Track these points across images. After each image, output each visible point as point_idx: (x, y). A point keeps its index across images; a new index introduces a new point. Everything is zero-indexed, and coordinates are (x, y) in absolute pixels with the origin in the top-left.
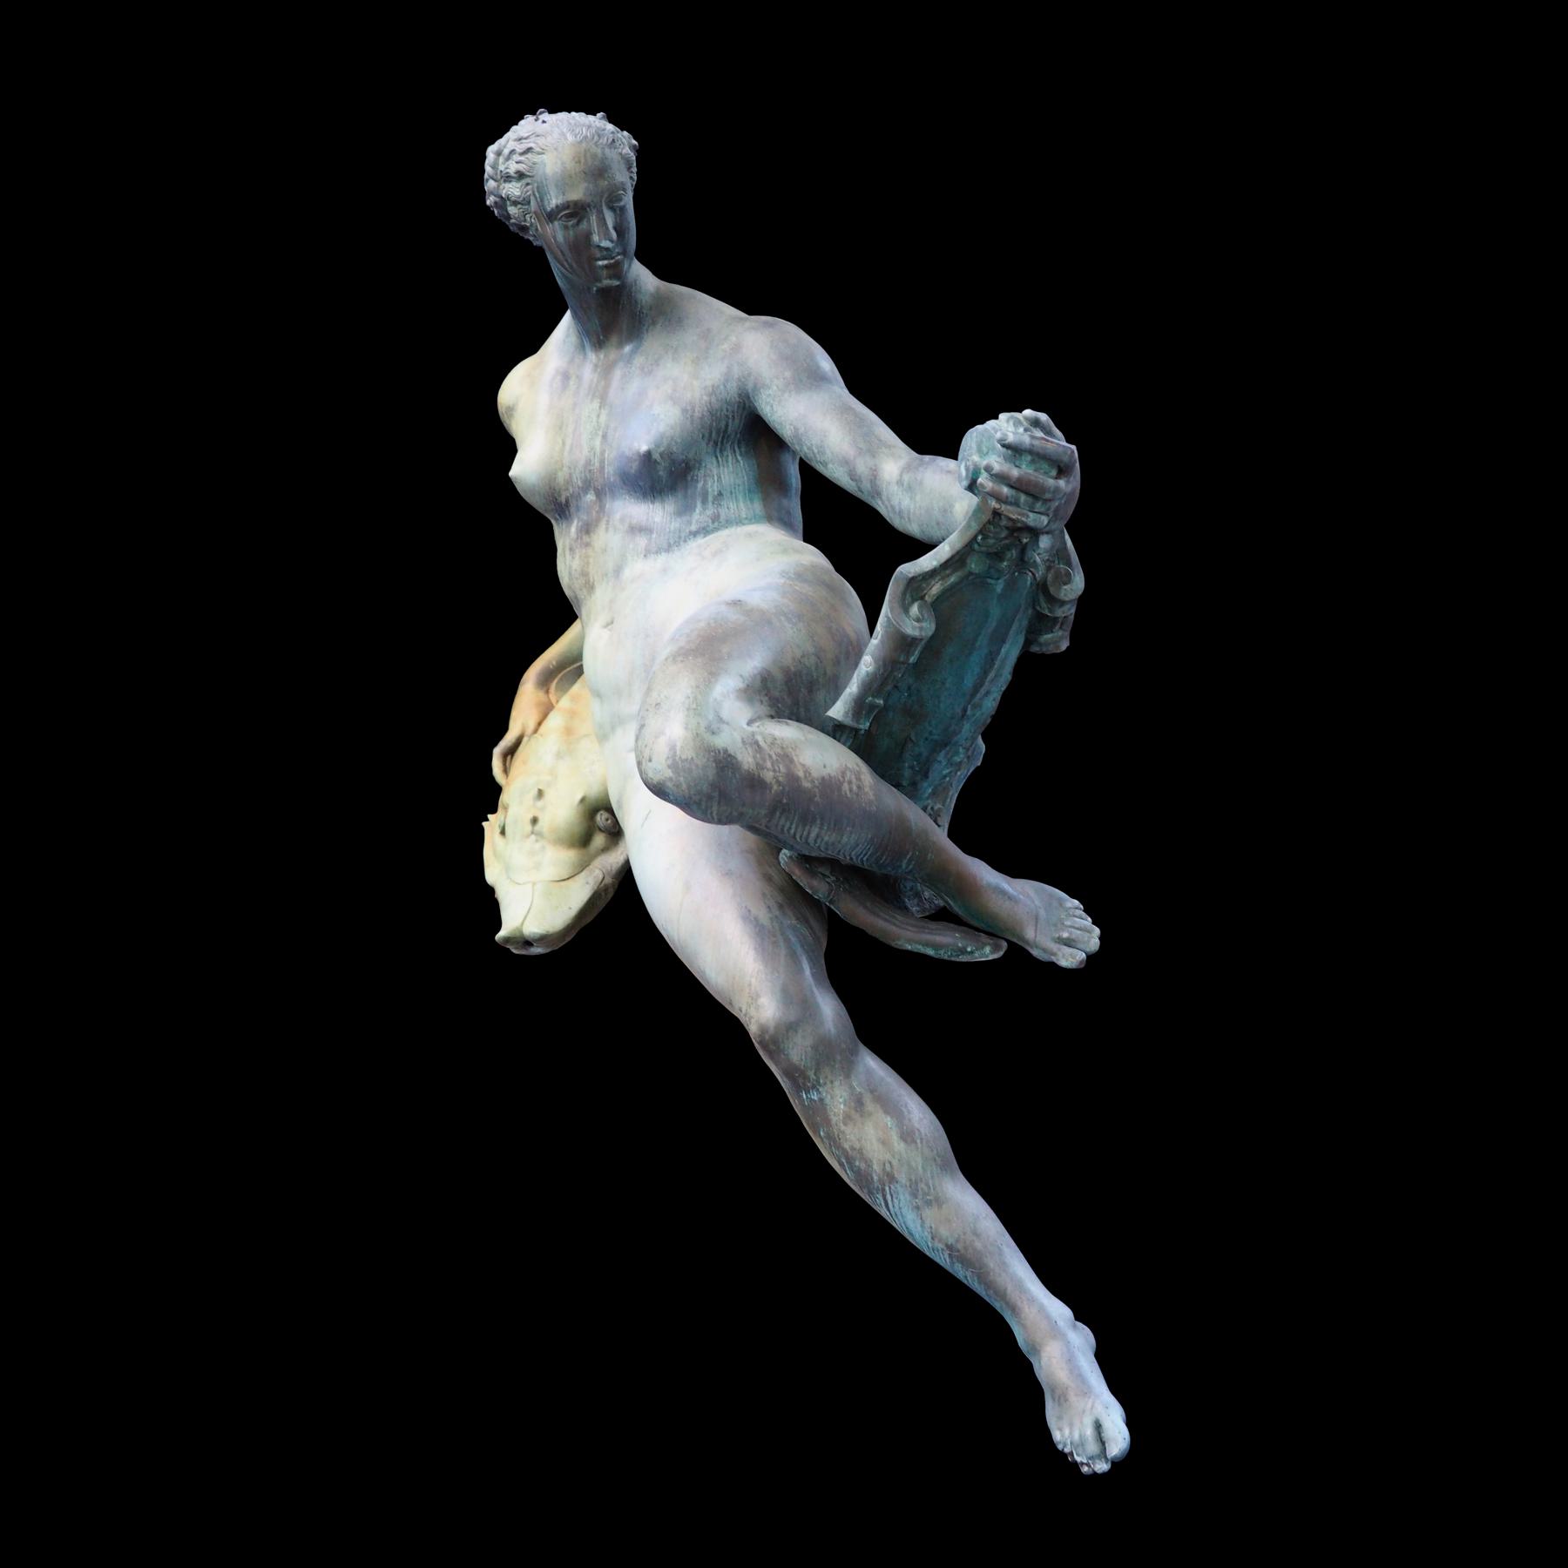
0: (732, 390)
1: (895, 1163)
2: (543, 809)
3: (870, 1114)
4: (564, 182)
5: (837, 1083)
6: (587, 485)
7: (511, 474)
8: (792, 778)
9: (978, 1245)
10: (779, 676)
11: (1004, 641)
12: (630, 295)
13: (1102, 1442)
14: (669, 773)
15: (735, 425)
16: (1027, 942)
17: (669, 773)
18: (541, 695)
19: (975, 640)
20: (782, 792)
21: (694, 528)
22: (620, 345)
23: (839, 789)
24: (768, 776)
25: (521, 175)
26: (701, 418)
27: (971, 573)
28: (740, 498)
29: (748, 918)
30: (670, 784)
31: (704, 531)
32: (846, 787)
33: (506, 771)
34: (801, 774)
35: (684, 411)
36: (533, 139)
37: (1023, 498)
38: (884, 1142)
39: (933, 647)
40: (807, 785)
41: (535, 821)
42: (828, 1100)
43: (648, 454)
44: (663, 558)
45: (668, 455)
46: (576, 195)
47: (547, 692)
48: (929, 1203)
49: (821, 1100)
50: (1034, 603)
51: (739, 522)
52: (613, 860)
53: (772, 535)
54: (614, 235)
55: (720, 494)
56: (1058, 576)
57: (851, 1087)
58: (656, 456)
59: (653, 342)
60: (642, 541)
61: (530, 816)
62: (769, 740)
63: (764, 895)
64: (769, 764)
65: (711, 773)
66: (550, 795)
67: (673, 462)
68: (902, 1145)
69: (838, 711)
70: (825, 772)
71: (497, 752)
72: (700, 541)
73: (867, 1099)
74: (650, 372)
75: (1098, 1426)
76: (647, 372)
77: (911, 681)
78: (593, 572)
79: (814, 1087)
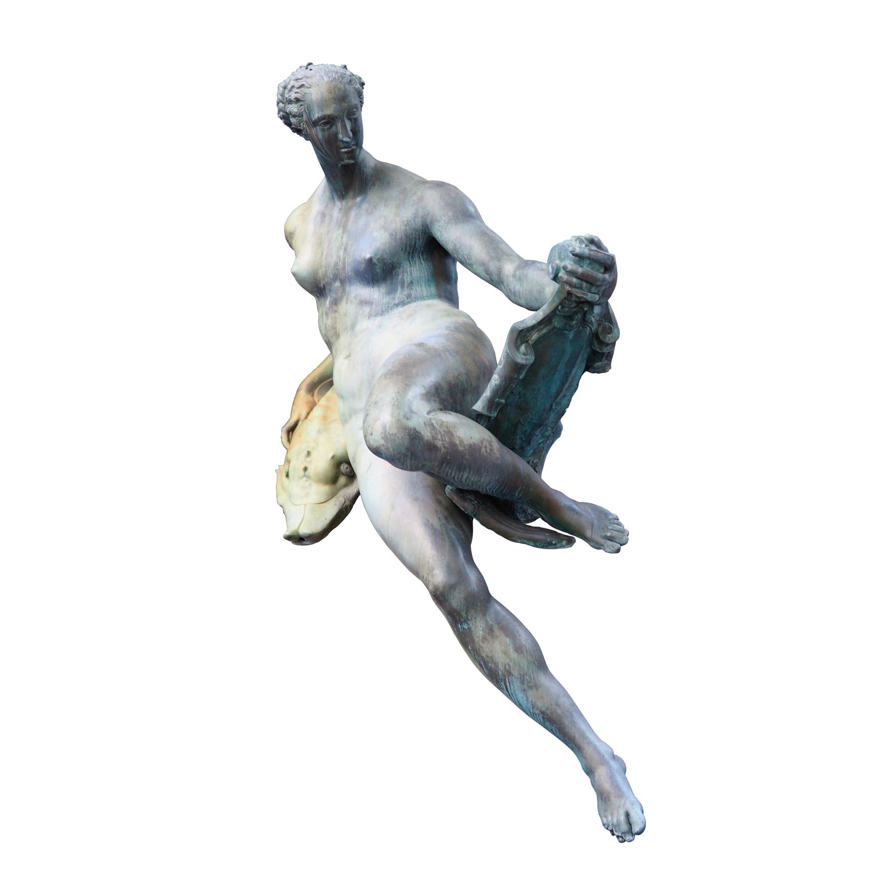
0: (418, 223)
1: (511, 664)
2: (310, 462)
3: (497, 637)
4: (322, 104)
5: (478, 619)
6: (336, 277)
8: (453, 444)
9: (559, 711)
10: (445, 386)
11: (574, 367)
12: (360, 169)
14: (382, 442)
15: (420, 243)
17: (382, 442)
18: (309, 397)
19: (557, 366)
20: (447, 453)
21: (396, 302)
22: (355, 197)
23: (480, 451)
24: (439, 443)
25: (298, 100)
26: (401, 239)
27: (555, 328)
28: (423, 284)
29: (427, 525)
30: (383, 448)
31: (403, 303)
32: (483, 450)
34: (458, 442)
35: (391, 235)
36: (304, 79)
37: (584, 284)
38: (505, 653)
39: (533, 370)
40: (461, 448)
41: (305, 469)
42: (473, 629)
44: (379, 319)
45: (382, 260)
46: (329, 111)
47: (313, 395)
48: (531, 688)
49: (469, 628)
51: (422, 298)
54: (351, 134)
55: (412, 282)
56: (604, 329)
57: (487, 621)
58: (375, 261)
59: (373, 195)
60: (367, 309)
61: (303, 466)
62: (440, 423)
63: (437, 511)
64: (439, 437)
65: (407, 442)
66: (314, 454)
67: (385, 264)
68: (516, 654)
69: (479, 406)
70: (471, 441)
72: (400, 309)
73: (496, 628)
74: (372, 213)
76: (370, 213)
77: (520, 389)
78: (339, 327)
79: (465, 621)
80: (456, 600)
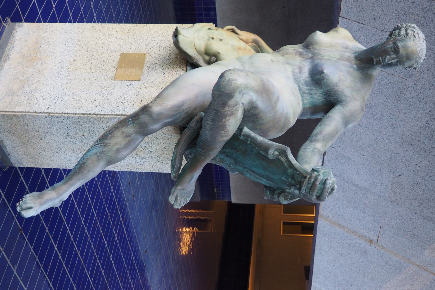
1: (110, 147)
3: (124, 139)
5: (134, 129)
6: (314, 54)
7: (317, 31)
8: (226, 116)
9: (85, 172)
10: (256, 112)
11: (267, 180)
14: (227, 79)
15: (332, 99)
16: (176, 187)
17: (227, 79)
18: (251, 40)
22: (356, 64)
23: (223, 130)
24: (226, 109)
25: (407, 34)
28: (310, 100)
29: (184, 103)
30: (224, 79)
31: (300, 90)
32: (223, 132)
33: (228, 30)
34: (227, 119)
35: (336, 84)
36: (418, 38)
37: (310, 185)
38: (116, 144)
40: (224, 120)
41: (213, 38)
42: (129, 127)
43: (323, 73)
45: (323, 79)
46: (401, 51)
47: (252, 42)
48: (98, 157)
49: (129, 125)
50: (279, 189)
51: (303, 100)
53: (299, 110)
54: (389, 62)
55: (311, 94)
56: (287, 196)
57: (133, 134)
58: (323, 75)
59: (357, 74)
60: (297, 71)
63: (191, 107)
64: (230, 109)
65: (227, 92)
67: (321, 80)
71: (234, 27)
74: (348, 73)
75: (30, 208)
79: (133, 122)
80: (144, 118)
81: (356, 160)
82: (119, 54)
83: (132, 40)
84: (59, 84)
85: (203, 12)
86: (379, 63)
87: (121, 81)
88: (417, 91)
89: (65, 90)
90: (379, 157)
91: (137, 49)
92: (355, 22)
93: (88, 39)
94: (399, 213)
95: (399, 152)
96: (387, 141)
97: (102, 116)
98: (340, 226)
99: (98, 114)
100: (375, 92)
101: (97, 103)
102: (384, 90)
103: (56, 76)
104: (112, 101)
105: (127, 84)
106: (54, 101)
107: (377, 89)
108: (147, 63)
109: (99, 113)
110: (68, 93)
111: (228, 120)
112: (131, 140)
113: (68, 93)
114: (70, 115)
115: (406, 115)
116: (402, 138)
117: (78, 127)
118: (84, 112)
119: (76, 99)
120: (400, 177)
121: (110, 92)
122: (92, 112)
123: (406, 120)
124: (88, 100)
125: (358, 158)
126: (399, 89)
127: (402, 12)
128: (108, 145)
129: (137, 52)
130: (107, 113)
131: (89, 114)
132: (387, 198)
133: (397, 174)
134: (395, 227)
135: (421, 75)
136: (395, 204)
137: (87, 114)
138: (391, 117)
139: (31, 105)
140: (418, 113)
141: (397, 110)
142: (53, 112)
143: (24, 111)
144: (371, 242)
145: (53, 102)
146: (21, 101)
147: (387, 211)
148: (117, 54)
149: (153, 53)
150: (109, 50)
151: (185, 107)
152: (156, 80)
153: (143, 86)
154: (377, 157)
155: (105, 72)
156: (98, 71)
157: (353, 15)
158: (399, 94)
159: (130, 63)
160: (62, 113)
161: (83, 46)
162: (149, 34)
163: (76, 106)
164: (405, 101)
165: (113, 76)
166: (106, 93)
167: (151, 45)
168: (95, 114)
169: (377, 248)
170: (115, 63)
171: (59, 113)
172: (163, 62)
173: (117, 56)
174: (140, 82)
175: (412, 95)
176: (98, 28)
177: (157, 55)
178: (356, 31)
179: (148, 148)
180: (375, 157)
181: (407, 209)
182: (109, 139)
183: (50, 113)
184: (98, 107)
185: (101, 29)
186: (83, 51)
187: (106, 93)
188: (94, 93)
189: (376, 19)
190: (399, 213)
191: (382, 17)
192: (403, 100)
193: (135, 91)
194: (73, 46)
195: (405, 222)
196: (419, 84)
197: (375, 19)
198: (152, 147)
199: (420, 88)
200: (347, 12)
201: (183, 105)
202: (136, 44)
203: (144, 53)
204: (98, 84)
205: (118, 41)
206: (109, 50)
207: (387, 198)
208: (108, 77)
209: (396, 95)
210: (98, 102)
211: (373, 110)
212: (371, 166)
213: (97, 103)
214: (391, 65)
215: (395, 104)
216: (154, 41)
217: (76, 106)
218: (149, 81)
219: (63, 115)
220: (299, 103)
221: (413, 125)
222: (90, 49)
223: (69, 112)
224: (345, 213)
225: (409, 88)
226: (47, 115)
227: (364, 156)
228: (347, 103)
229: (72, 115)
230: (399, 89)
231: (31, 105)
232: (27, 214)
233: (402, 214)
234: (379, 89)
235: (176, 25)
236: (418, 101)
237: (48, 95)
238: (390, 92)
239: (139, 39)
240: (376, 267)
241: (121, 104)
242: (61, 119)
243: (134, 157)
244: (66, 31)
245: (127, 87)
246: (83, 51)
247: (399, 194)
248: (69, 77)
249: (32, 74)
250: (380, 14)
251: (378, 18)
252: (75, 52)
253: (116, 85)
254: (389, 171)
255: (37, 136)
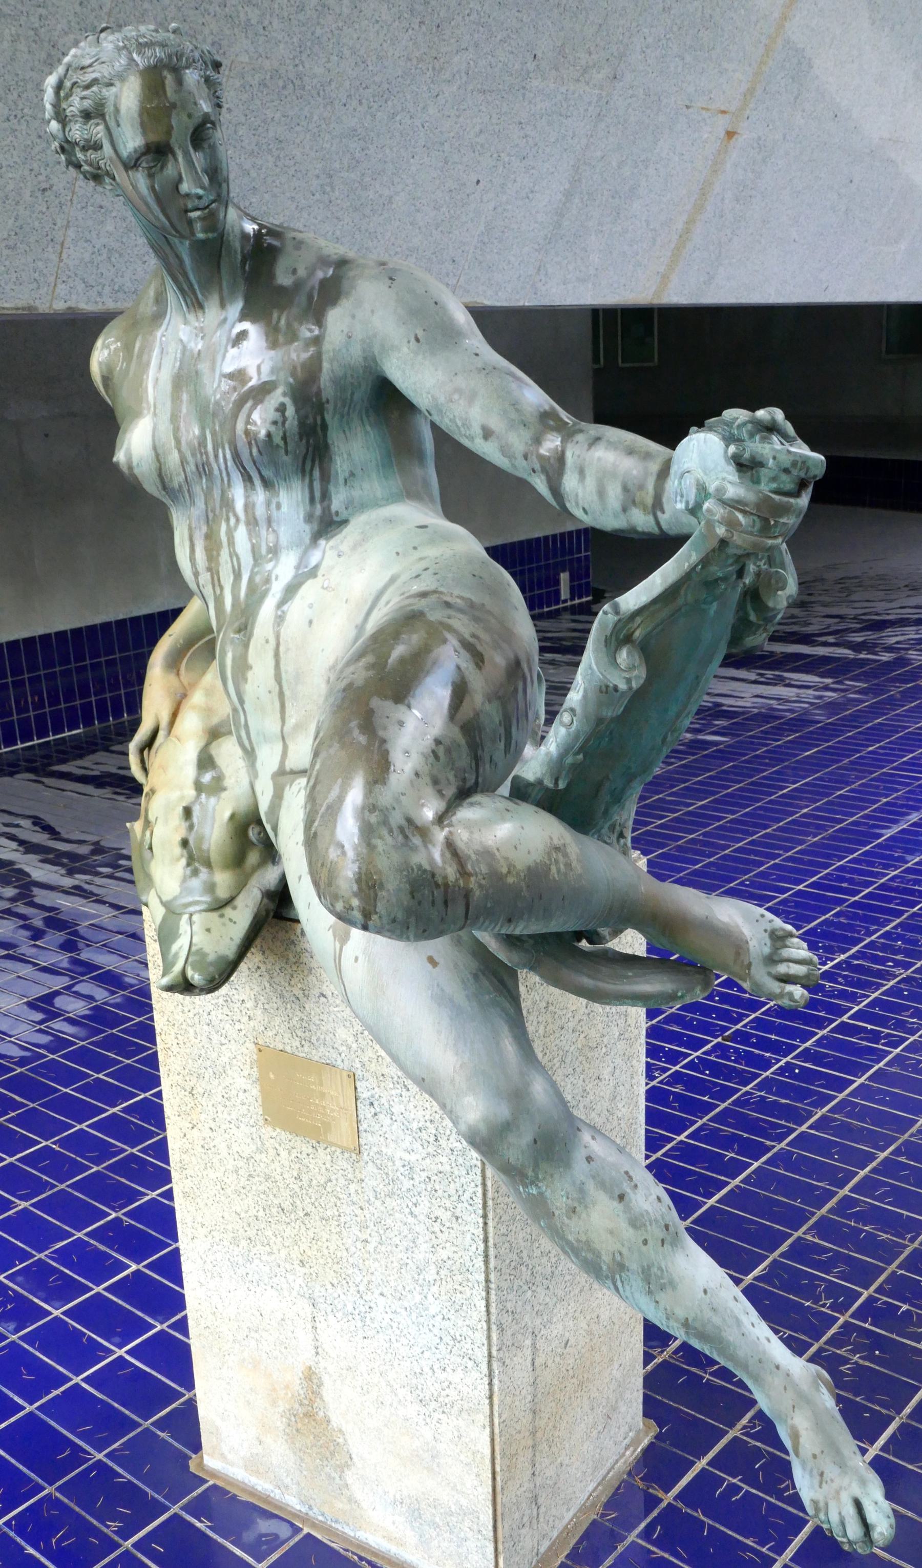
1: (625, 1251)
7: (120, 457)
9: (716, 1320)
13: (867, 1527)
15: (361, 394)
18: (172, 677)
28: (374, 475)
29: (441, 999)
32: (554, 869)
33: (145, 770)
36: (97, 66)
39: (638, 697)
42: (548, 1194)
47: (178, 674)
48: (662, 1288)
49: (541, 1194)
50: (741, 606)
51: (376, 504)
52: (269, 877)
53: (413, 514)
54: (206, 180)
55: (352, 474)
63: (456, 966)
68: (631, 1231)
71: (133, 746)
73: (590, 1186)
75: (858, 1506)
79: (532, 1183)
80: (518, 1147)
81: (491, 206)
82: (268, 1131)
83: (216, 1082)
84: (387, 1317)
85: (88, 662)
86: (212, 221)
87: (363, 1134)
88: (266, 23)
89: (406, 1304)
90: (481, 131)
91: (246, 1073)
92: (64, 256)
93: (226, 1215)
94: (648, 51)
95: (463, 67)
96: (432, 111)
97: (490, 1203)
98: (685, 235)
99: (485, 1216)
100: (280, 164)
101: (445, 1216)
102: (271, 134)
103: (359, 1324)
104: (435, 1169)
105: (369, 1116)
106: (447, 1339)
107: (269, 157)
108: (292, 1045)
109: (481, 1212)
110: (418, 1298)
111: (511, 866)
112: (593, 1177)
113: (418, 1298)
114: (493, 1297)
115: (347, 52)
116: (420, 60)
117: (526, 1258)
118: (481, 1258)
119: (438, 1278)
120: (539, 55)
121: (402, 1170)
122: (480, 1232)
123: (362, 52)
124: (435, 1241)
125: (485, 199)
126: (265, 86)
127: (10, 97)
128: (618, 1258)
129: (255, 1073)
130: (480, 1190)
131: (486, 1241)
132: (604, 94)
133: (531, 66)
134: (688, 58)
135: (211, 10)
136: (622, 65)
137: (486, 1247)
138: (355, 103)
139: (466, 1407)
140: (338, 12)
141: (333, 85)
142: (485, 1348)
143: (488, 1430)
144: (730, 134)
145: (452, 1343)
146: (456, 1434)
147: (641, 91)
148: (268, 1135)
149: (252, 1023)
150: (258, 1157)
151: (460, 997)
152: (348, 1024)
153: (373, 1067)
154: (481, 139)
155: (333, 1178)
156: (333, 1199)
157: (40, 264)
158: (281, 83)
159: (295, 1097)
160: (488, 1322)
161: (251, 1233)
162: (191, 1031)
163: (459, 1278)
164: (302, 63)
165: (346, 1155)
166: (407, 1184)
167: (227, 1026)
168: (485, 1224)
169: (748, 112)
170: (303, 1146)
171: (489, 1329)
172: (282, 996)
173: (274, 1134)
174: (359, 1073)
175: (280, 37)
176: (188, 1183)
177: (259, 1012)
178: (90, 249)
179: (577, 1019)
180: (482, 146)
181: (634, 24)
182: (599, 1256)
183: (490, 1356)
184: (458, 1214)
185: (189, 1172)
186: (269, 1233)
187: (407, 1184)
188: (410, 1220)
189: (44, 185)
190: (648, 51)
191: (35, 166)
192: (301, 67)
193: (393, 1092)
194: (257, 1262)
195: (675, 29)
196: (242, 15)
197: (44, 190)
198: (574, 1008)
199: (257, 12)
200: (35, 285)
201: (451, 1000)
202: (229, 1072)
203: (256, 1050)
204: (378, 1203)
205: (224, 1127)
206: (258, 1157)
207: (604, 94)
208: (350, 1170)
209: (286, 92)
210: (439, 1212)
211: (337, 165)
212: (509, 155)
213: (445, 1216)
214: (215, 175)
215: (314, 92)
216: (213, 1017)
217: (459, 1278)
218: (354, 1046)
219: (493, 1318)
220: (390, 521)
221: (377, 27)
222: (261, 1213)
223: (483, 1303)
224: (648, 222)
225: (261, 50)
226: (495, 1365)
227: (478, 182)
228: (375, 336)
229: (493, 1292)
230: (265, 86)
231: (466, 1407)
232: (882, 1518)
233: (650, 40)
234: (270, 151)
235: (155, 992)
236: (301, 17)
237: (427, 1354)
238: (278, 115)
239: (208, 1063)
240: (804, 111)
241: (443, 1142)
242: (507, 1319)
243: (604, 1050)
244: (209, 1275)
245: (381, 1117)
246: (269, 1233)
247: (590, 54)
248: (362, 1288)
249: (359, 1389)
250: (27, 173)
251: (41, 178)
252: (273, 1257)
253: (375, 1149)
254: (524, 95)
255: (557, 1359)
